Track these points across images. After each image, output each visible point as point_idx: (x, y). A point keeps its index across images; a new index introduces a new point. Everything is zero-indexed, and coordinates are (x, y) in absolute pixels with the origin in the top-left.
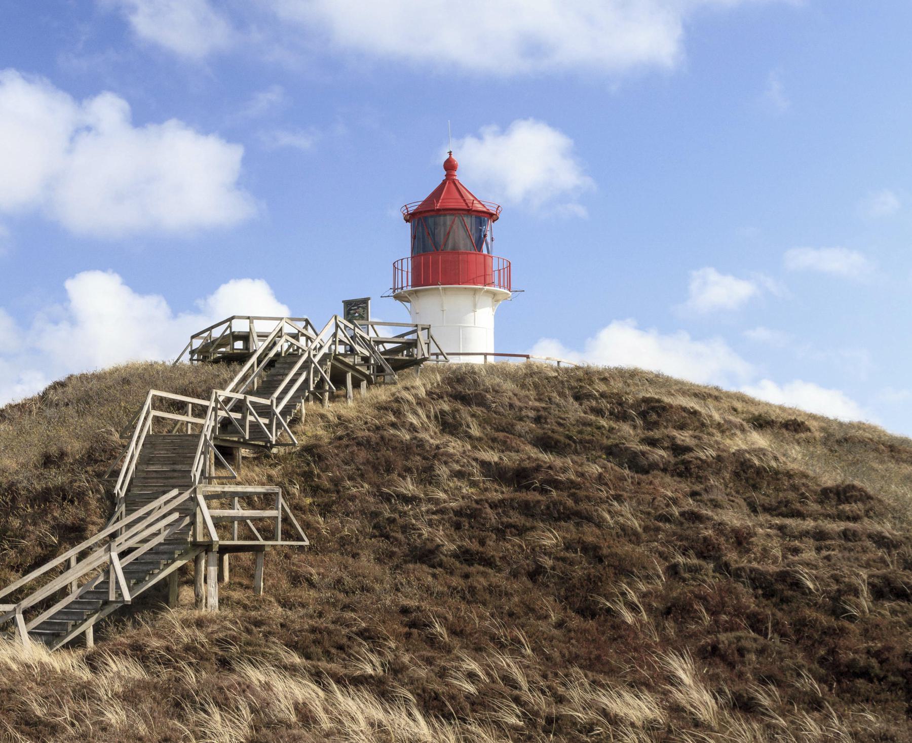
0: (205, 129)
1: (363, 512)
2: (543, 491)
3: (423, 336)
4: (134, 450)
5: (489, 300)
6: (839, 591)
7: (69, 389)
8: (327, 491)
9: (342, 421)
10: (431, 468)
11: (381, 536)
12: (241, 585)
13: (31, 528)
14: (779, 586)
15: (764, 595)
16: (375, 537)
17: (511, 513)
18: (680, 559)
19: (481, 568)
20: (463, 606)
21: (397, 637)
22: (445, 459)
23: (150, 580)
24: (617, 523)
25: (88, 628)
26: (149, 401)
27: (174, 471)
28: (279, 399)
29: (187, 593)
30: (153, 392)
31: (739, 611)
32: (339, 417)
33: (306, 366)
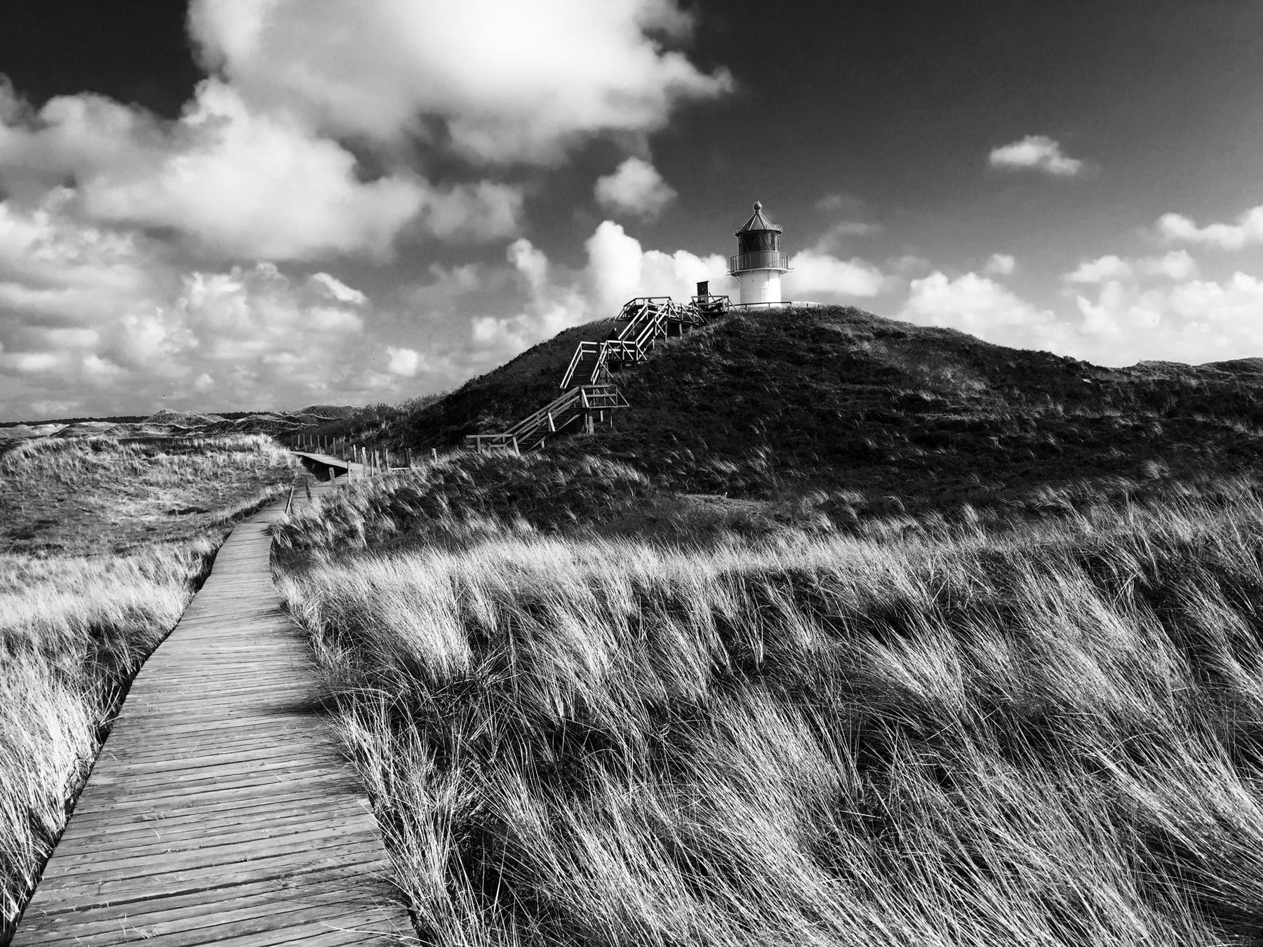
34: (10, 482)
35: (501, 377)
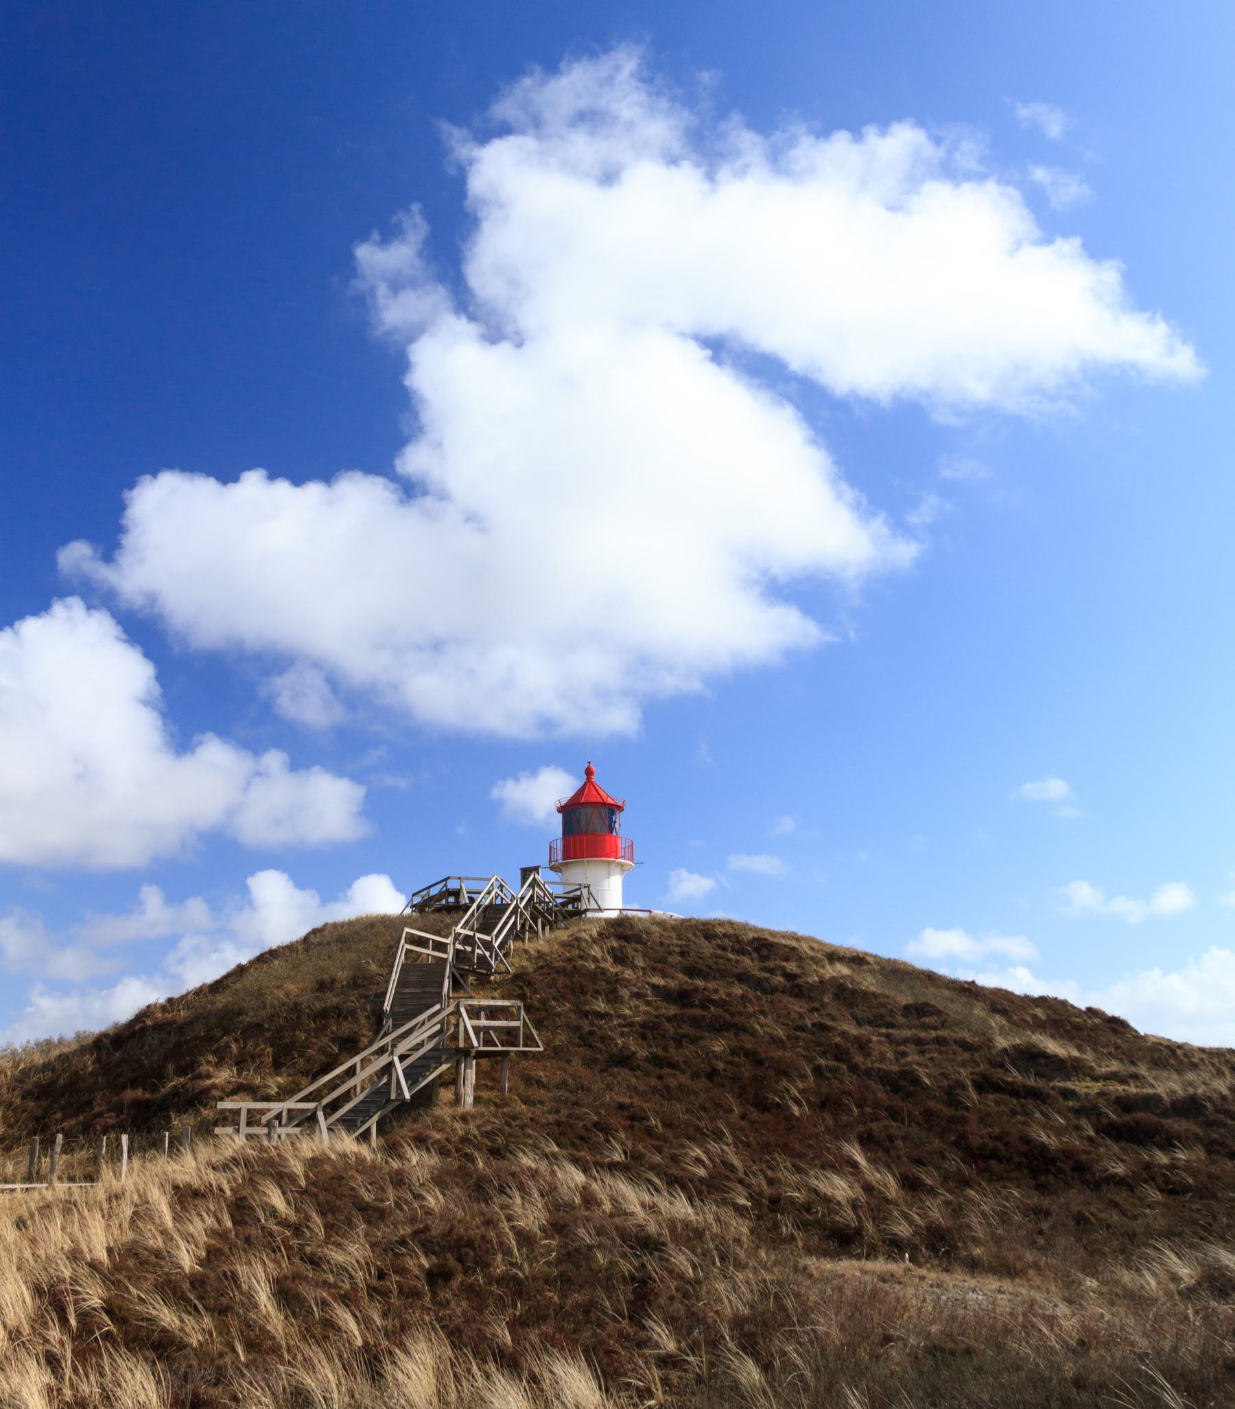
0: (339, 772)
1: (568, 1026)
2: (704, 1007)
3: (585, 891)
4: (395, 976)
5: (618, 870)
6: (949, 1086)
7: (326, 933)
8: (538, 1010)
9: (540, 955)
10: (614, 991)
11: (585, 1045)
12: (487, 1086)
13: (314, 1040)
14: (903, 1083)
15: (892, 1090)
16: (579, 1046)
17: (683, 1025)
18: (823, 1062)
19: (670, 1071)
20: (665, 1103)
21: (624, 1128)
22: (624, 983)
23: (423, 1081)
24: (766, 1032)
25: (372, 1123)
26: (403, 940)
27: (425, 992)
28: (497, 936)
29: (446, 1095)
30: (407, 930)
31: (877, 1105)
32: (538, 952)
33: (514, 912)
34: (1205, 1205)
35: (222, 1000)
